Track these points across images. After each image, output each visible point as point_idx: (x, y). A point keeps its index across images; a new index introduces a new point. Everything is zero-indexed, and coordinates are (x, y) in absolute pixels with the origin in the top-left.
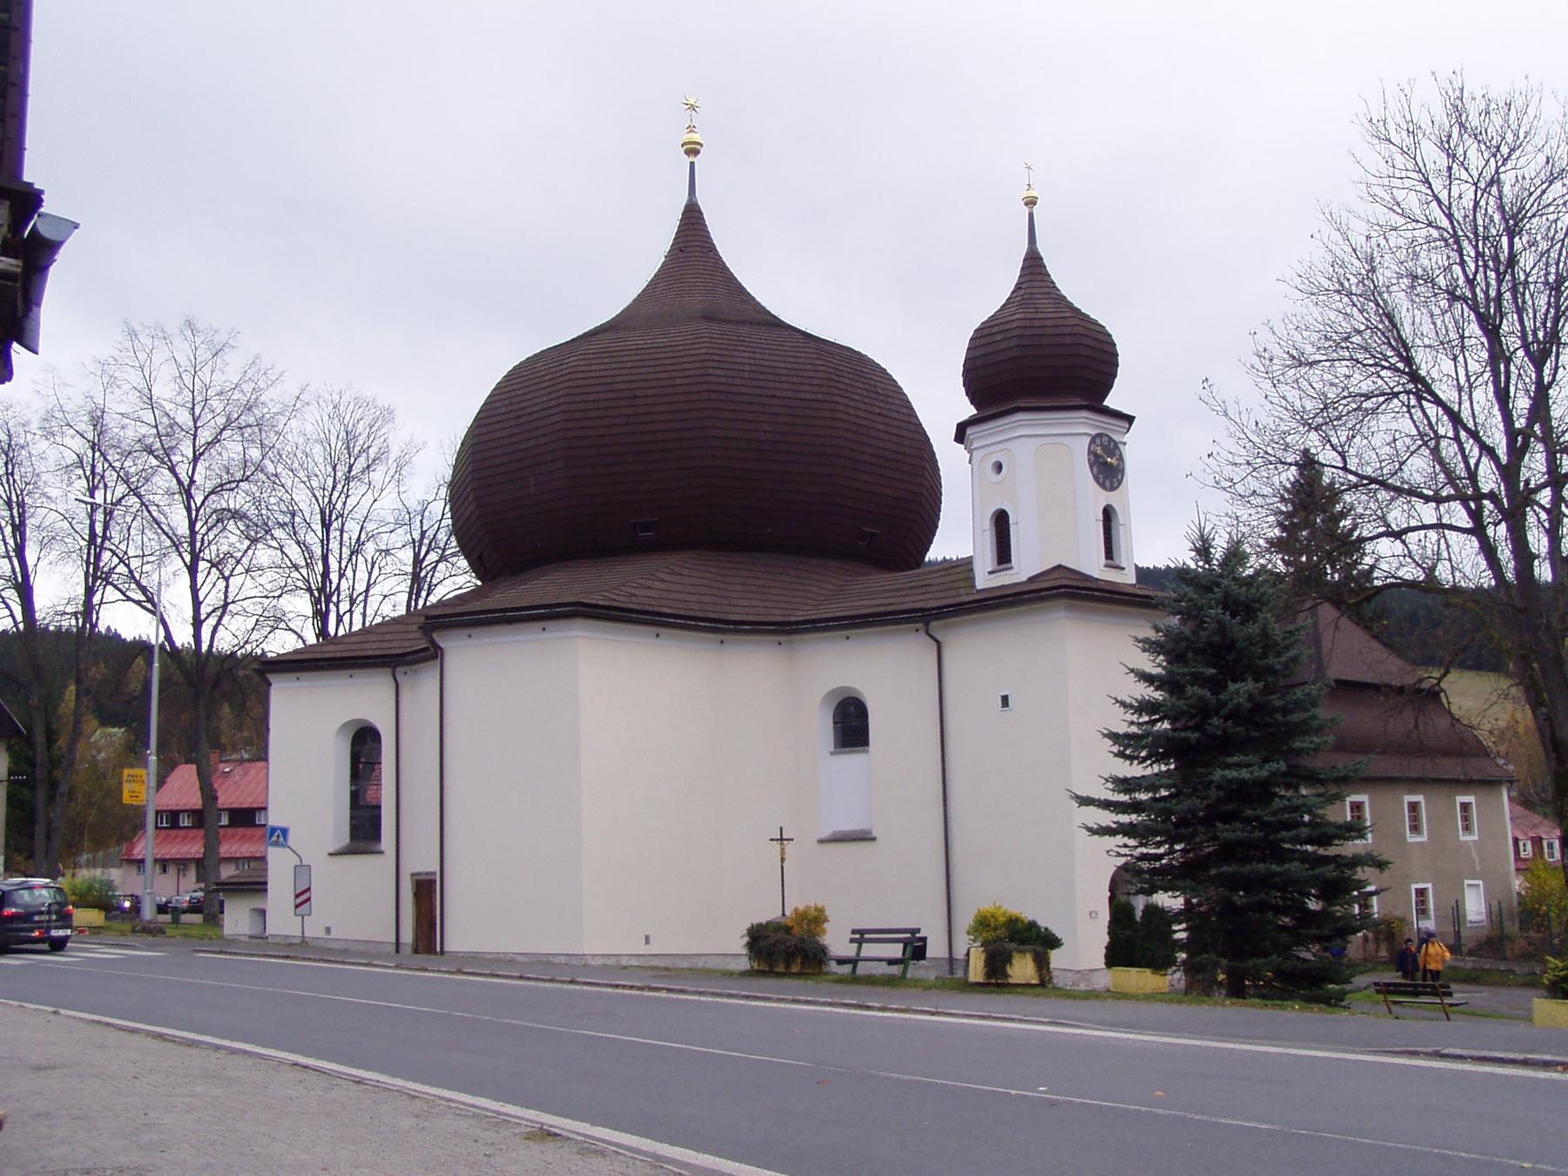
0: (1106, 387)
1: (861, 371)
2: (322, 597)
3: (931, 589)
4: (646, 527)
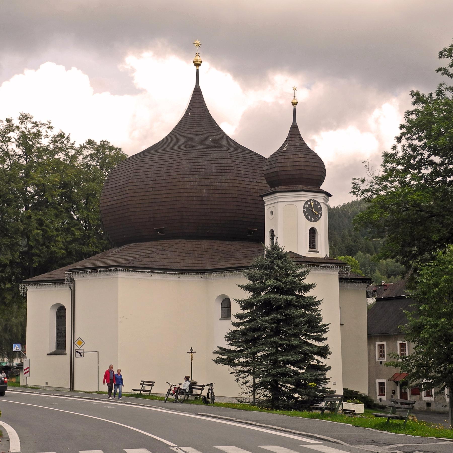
4: (161, 231)
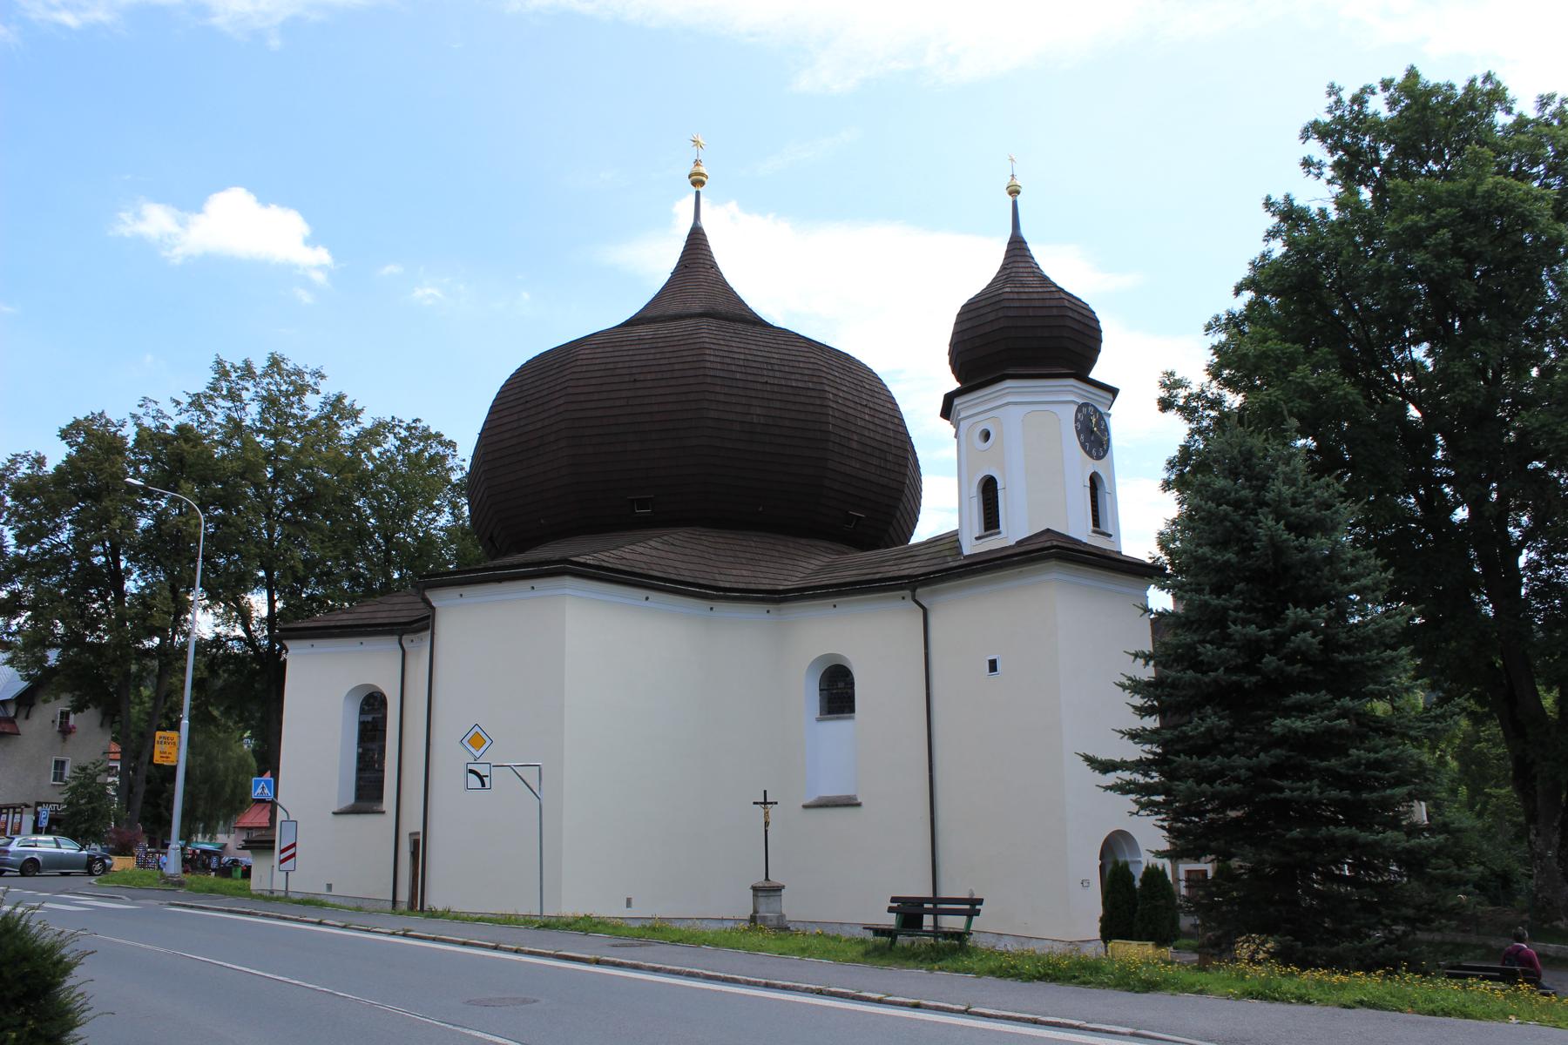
0: (1091, 360)
1: (850, 368)
3: (917, 559)
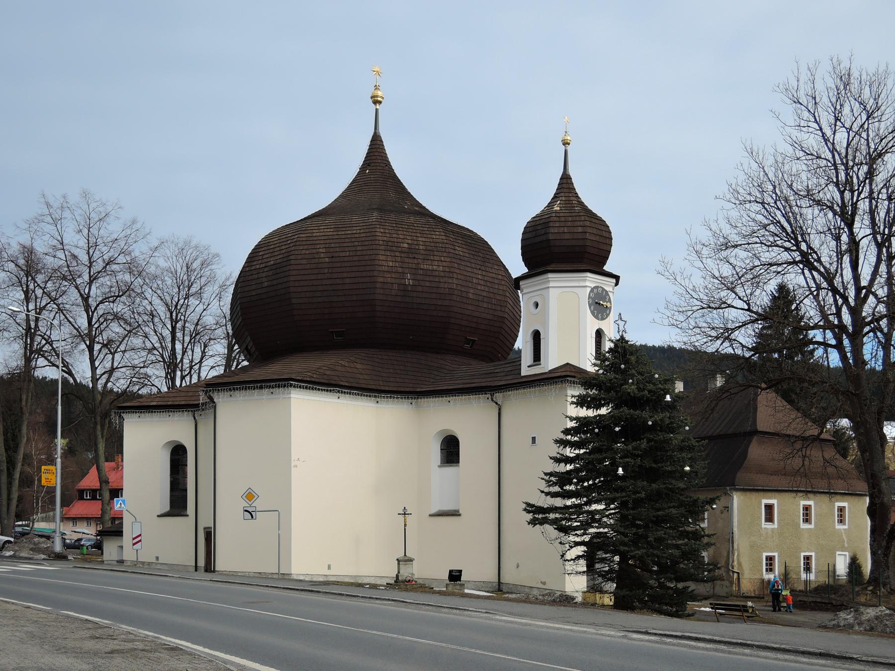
2: (172, 366)
